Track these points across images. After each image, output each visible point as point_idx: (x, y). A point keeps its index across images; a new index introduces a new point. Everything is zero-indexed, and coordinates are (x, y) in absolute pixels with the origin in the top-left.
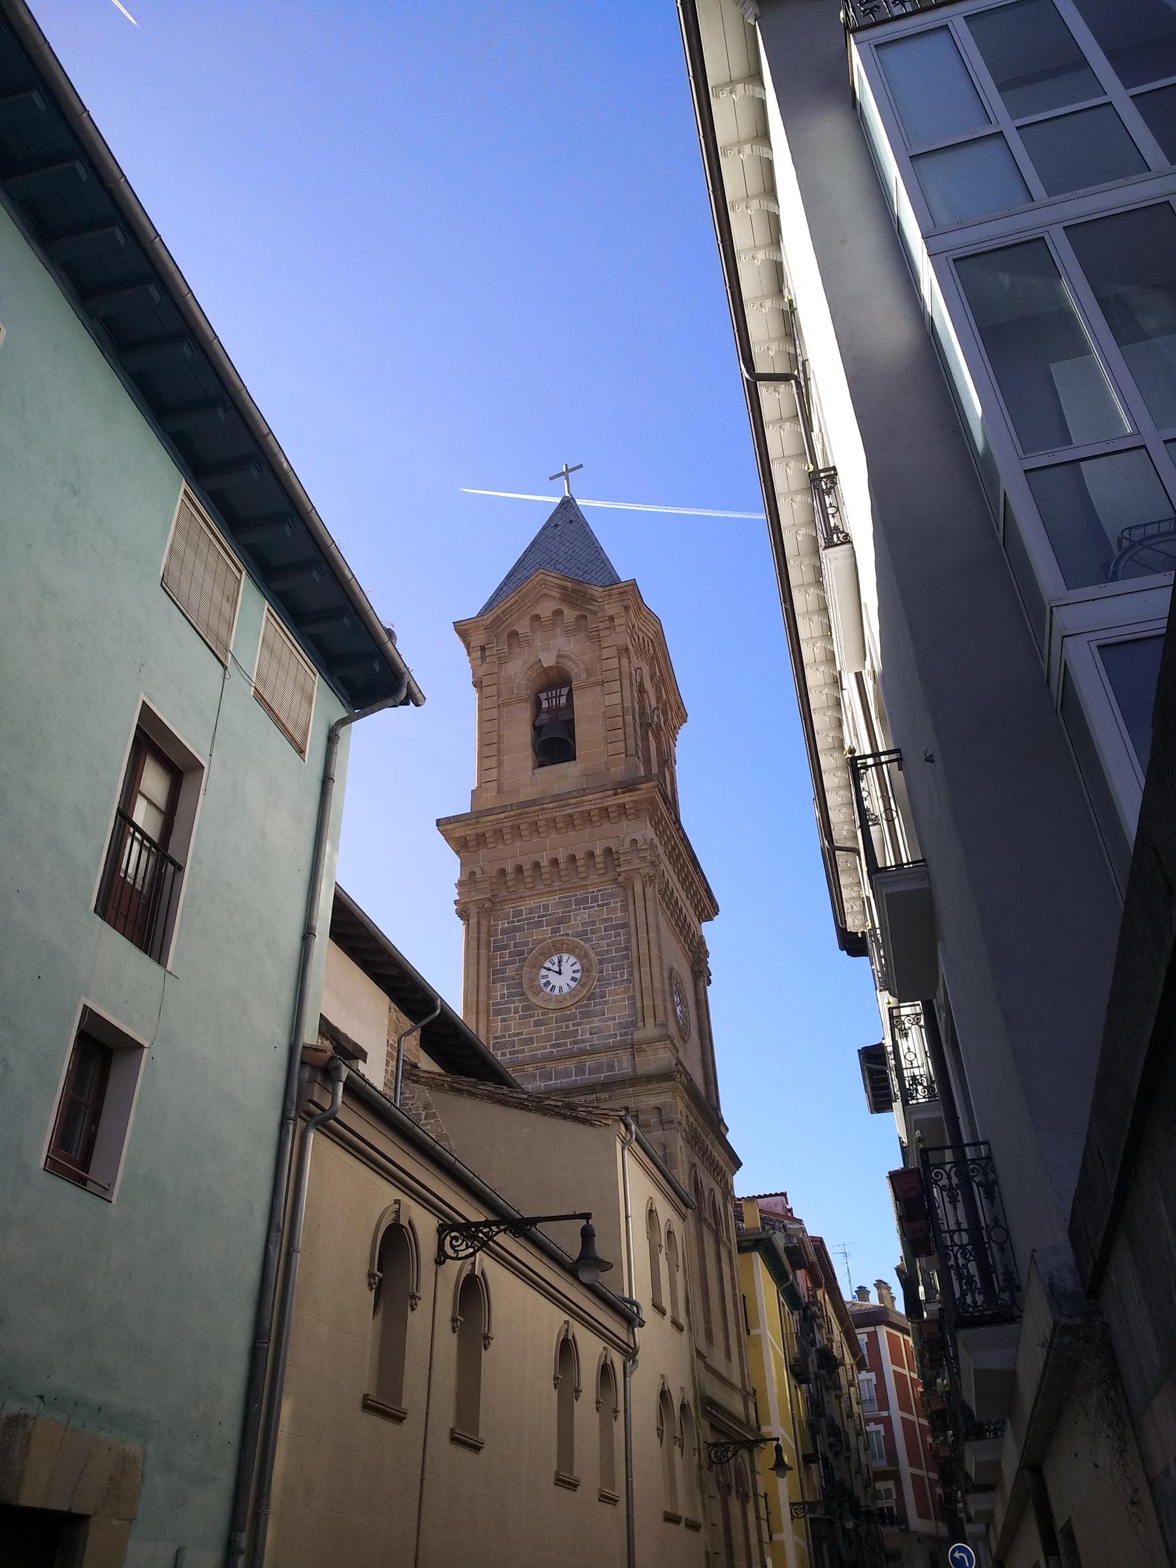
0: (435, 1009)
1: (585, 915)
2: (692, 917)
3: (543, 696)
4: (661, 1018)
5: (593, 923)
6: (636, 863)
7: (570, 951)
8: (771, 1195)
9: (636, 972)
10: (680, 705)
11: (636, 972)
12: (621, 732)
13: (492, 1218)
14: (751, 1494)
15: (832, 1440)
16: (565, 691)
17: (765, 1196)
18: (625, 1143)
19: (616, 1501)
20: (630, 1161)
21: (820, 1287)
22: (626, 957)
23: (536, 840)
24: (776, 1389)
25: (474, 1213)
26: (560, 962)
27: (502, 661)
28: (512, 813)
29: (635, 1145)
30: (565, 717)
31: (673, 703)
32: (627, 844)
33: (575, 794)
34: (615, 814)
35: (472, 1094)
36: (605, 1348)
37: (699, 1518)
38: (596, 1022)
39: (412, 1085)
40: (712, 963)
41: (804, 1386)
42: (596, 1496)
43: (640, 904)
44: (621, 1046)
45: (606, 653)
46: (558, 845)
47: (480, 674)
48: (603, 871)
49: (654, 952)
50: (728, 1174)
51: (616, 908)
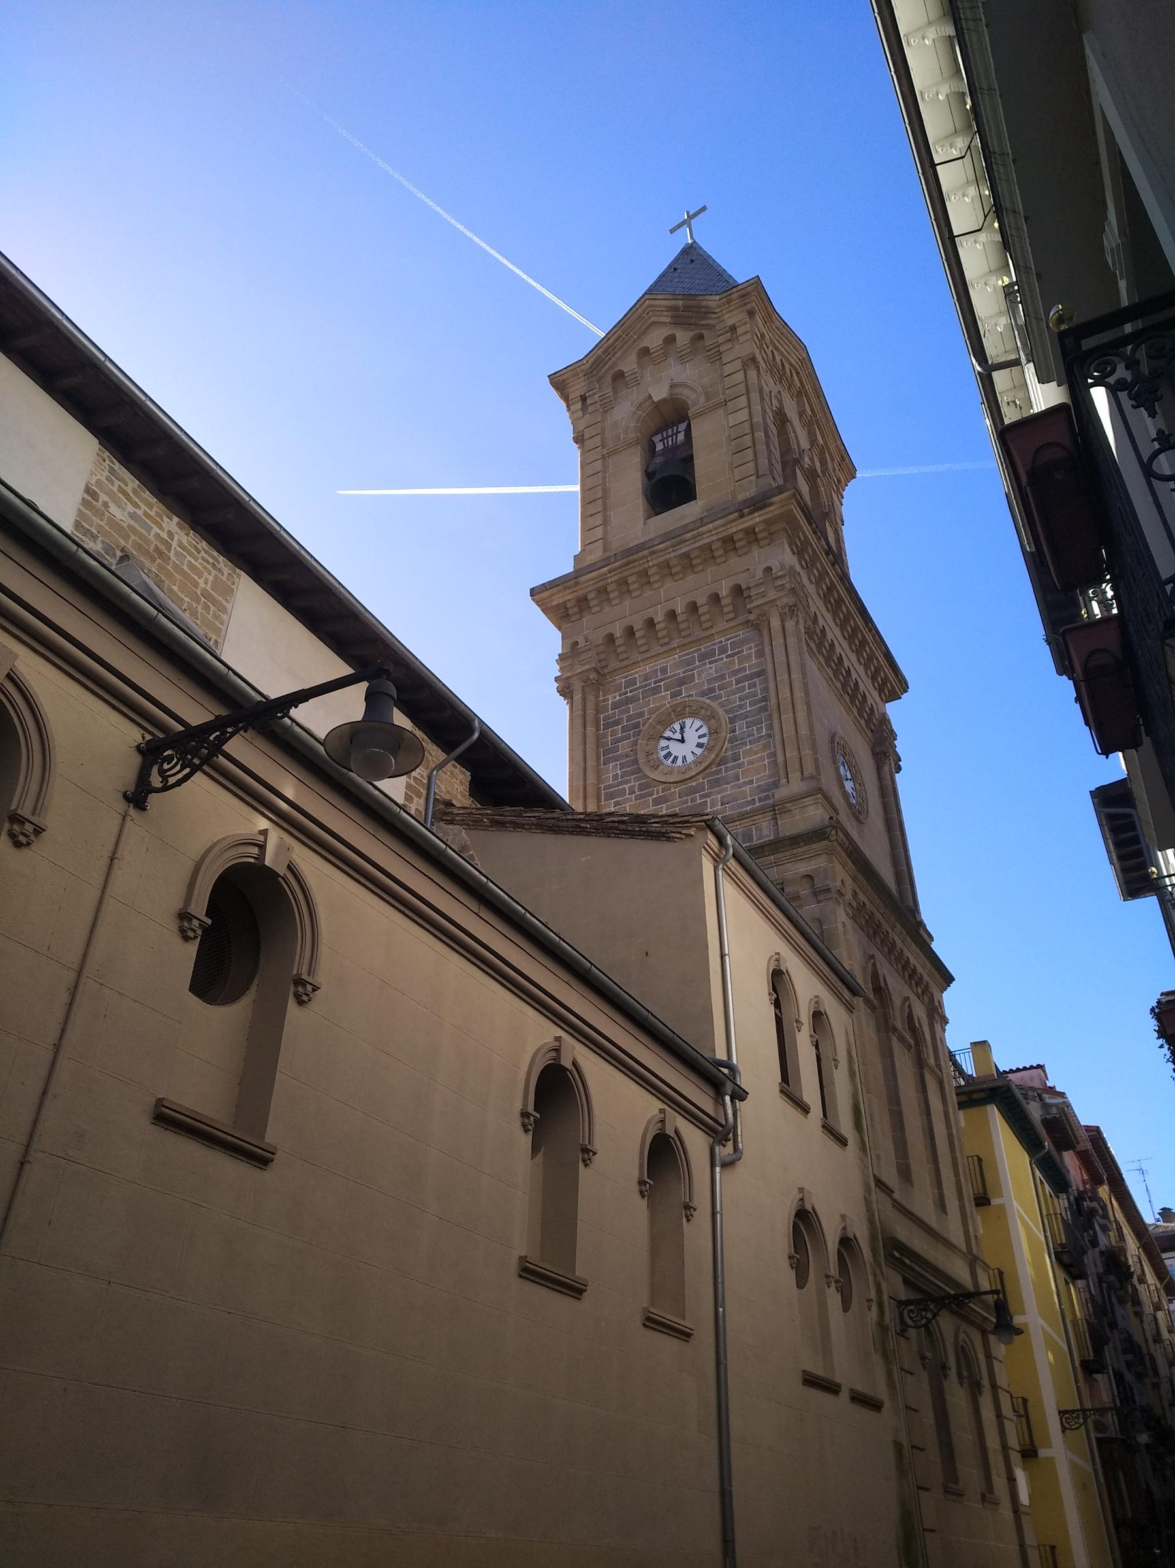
0: (472, 731)
1: (711, 670)
2: (873, 696)
3: (657, 438)
4: (809, 770)
5: (722, 677)
6: (772, 594)
7: (694, 715)
8: (1025, 1069)
9: (776, 723)
10: (844, 455)
11: (776, 723)
12: (750, 451)
13: (224, 712)
14: (986, 1382)
15: (1130, 1357)
16: (683, 427)
17: (1018, 1070)
18: (717, 860)
19: (688, 1335)
20: (729, 890)
21: (1101, 1183)
22: (765, 709)
23: (648, 593)
24: (1030, 1271)
25: (195, 710)
26: (682, 728)
27: (607, 407)
28: (617, 564)
29: (732, 864)
30: (684, 455)
31: (834, 451)
32: (759, 574)
33: (691, 526)
34: (743, 543)
35: (517, 826)
36: (662, 1111)
37: (880, 1391)
38: (729, 790)
39: (446, 826)
40: (901, 746)
41: (1080, 1283)
42: (638, 1320)
43: (778, 641)
44: (761, 811)
45: (728, 369)
46: (675, 594)
47: (582, 427)
48: (732, 615)
49: (799, 694)
50: (934, 989)
51: (750, 655)
